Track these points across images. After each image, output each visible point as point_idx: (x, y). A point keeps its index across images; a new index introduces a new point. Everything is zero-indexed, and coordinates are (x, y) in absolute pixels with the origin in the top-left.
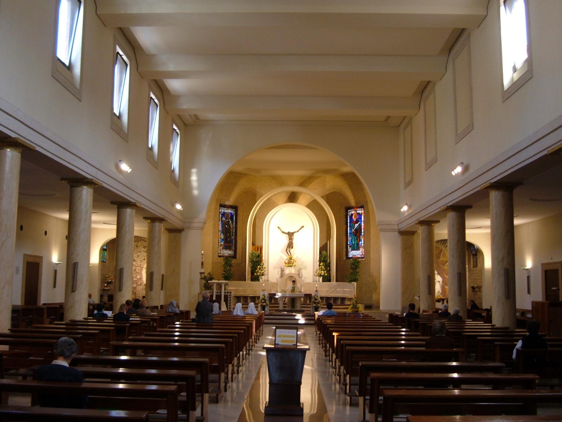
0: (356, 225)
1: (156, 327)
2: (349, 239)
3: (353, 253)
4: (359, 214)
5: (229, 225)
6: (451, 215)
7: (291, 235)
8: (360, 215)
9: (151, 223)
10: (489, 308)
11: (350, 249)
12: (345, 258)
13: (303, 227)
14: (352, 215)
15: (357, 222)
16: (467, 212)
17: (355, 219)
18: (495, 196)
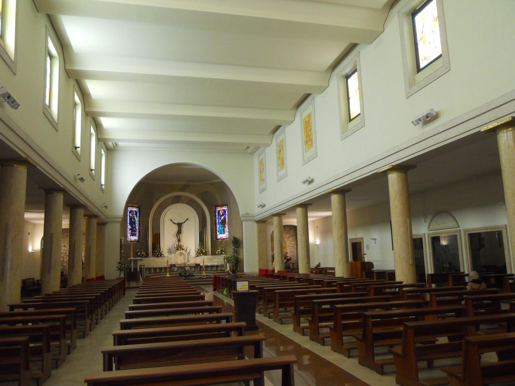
0: (223, 217)
1: (33, 339)
2: (218, 226)
3: (220, 236)
4: (224, 210)
5: (134, 219)
6: (299, 210)
7: (180, 225)
8: (225, 211)
9: (87, 219)
10: (9, 307)
11: (218, 233)
12: (215, 239)
13: (187, 219)
14: (219, 211)
15: (223, 215)
16: (309, 207)
17: (221, 214)
18: (335, 198)
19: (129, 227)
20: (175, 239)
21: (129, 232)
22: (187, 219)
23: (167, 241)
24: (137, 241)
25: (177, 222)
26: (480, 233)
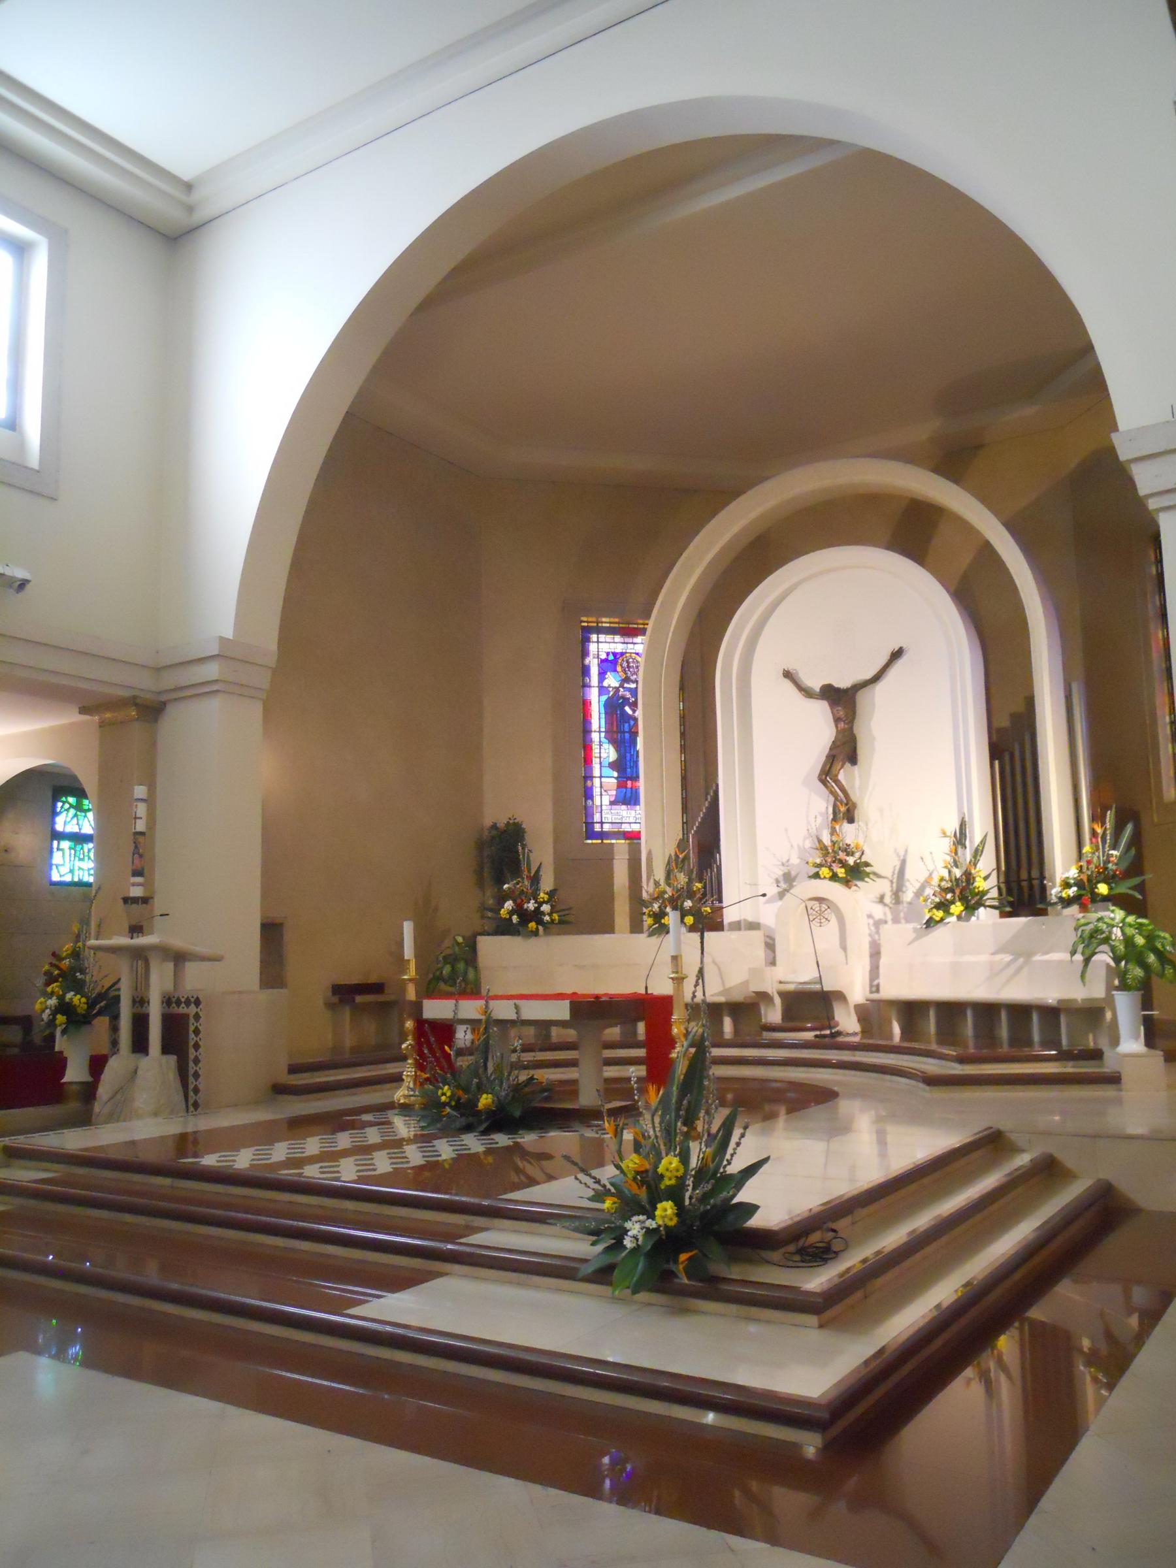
13: (897, 655)
19: (609, 753)
20: (820, 804)
21: (604, 782)
22: (897, 655)
23: (770, 816)
24: (589, 824)
25: (816, 685)
26: (937, 470)
